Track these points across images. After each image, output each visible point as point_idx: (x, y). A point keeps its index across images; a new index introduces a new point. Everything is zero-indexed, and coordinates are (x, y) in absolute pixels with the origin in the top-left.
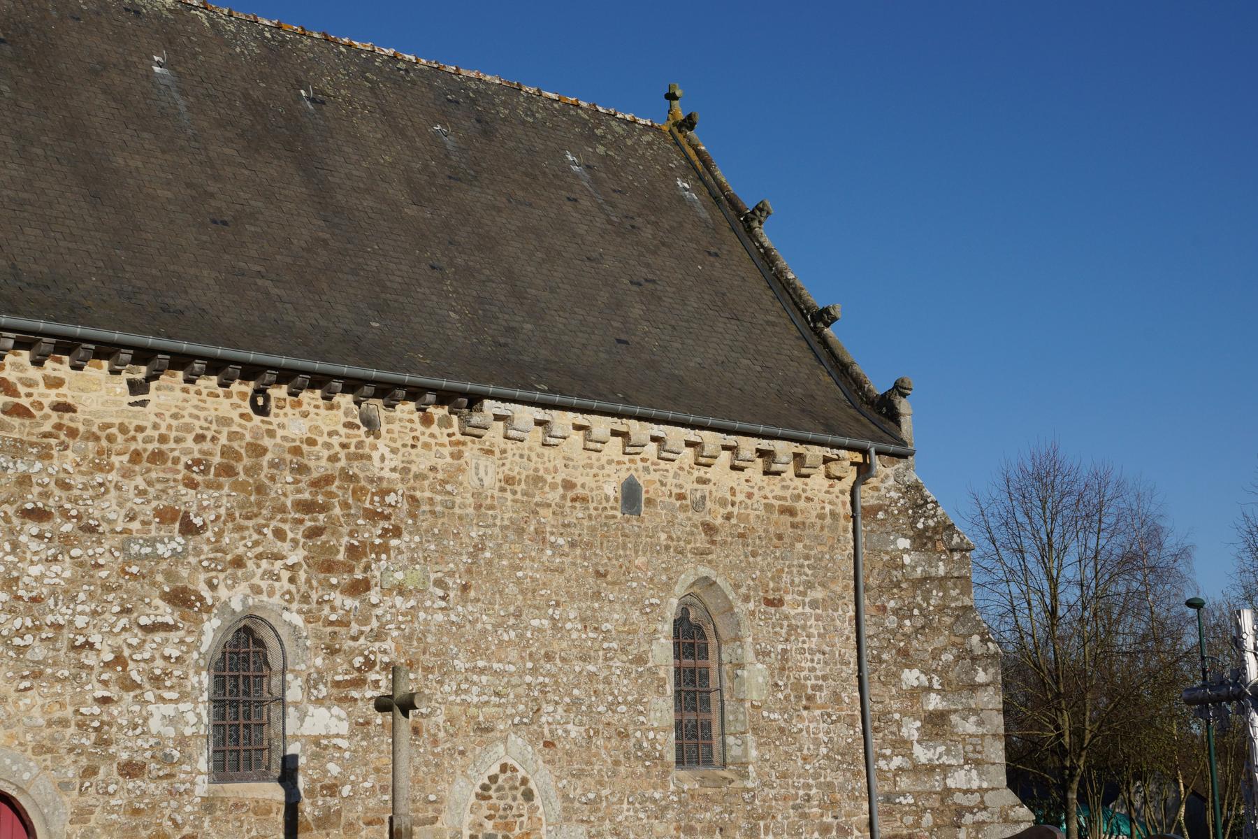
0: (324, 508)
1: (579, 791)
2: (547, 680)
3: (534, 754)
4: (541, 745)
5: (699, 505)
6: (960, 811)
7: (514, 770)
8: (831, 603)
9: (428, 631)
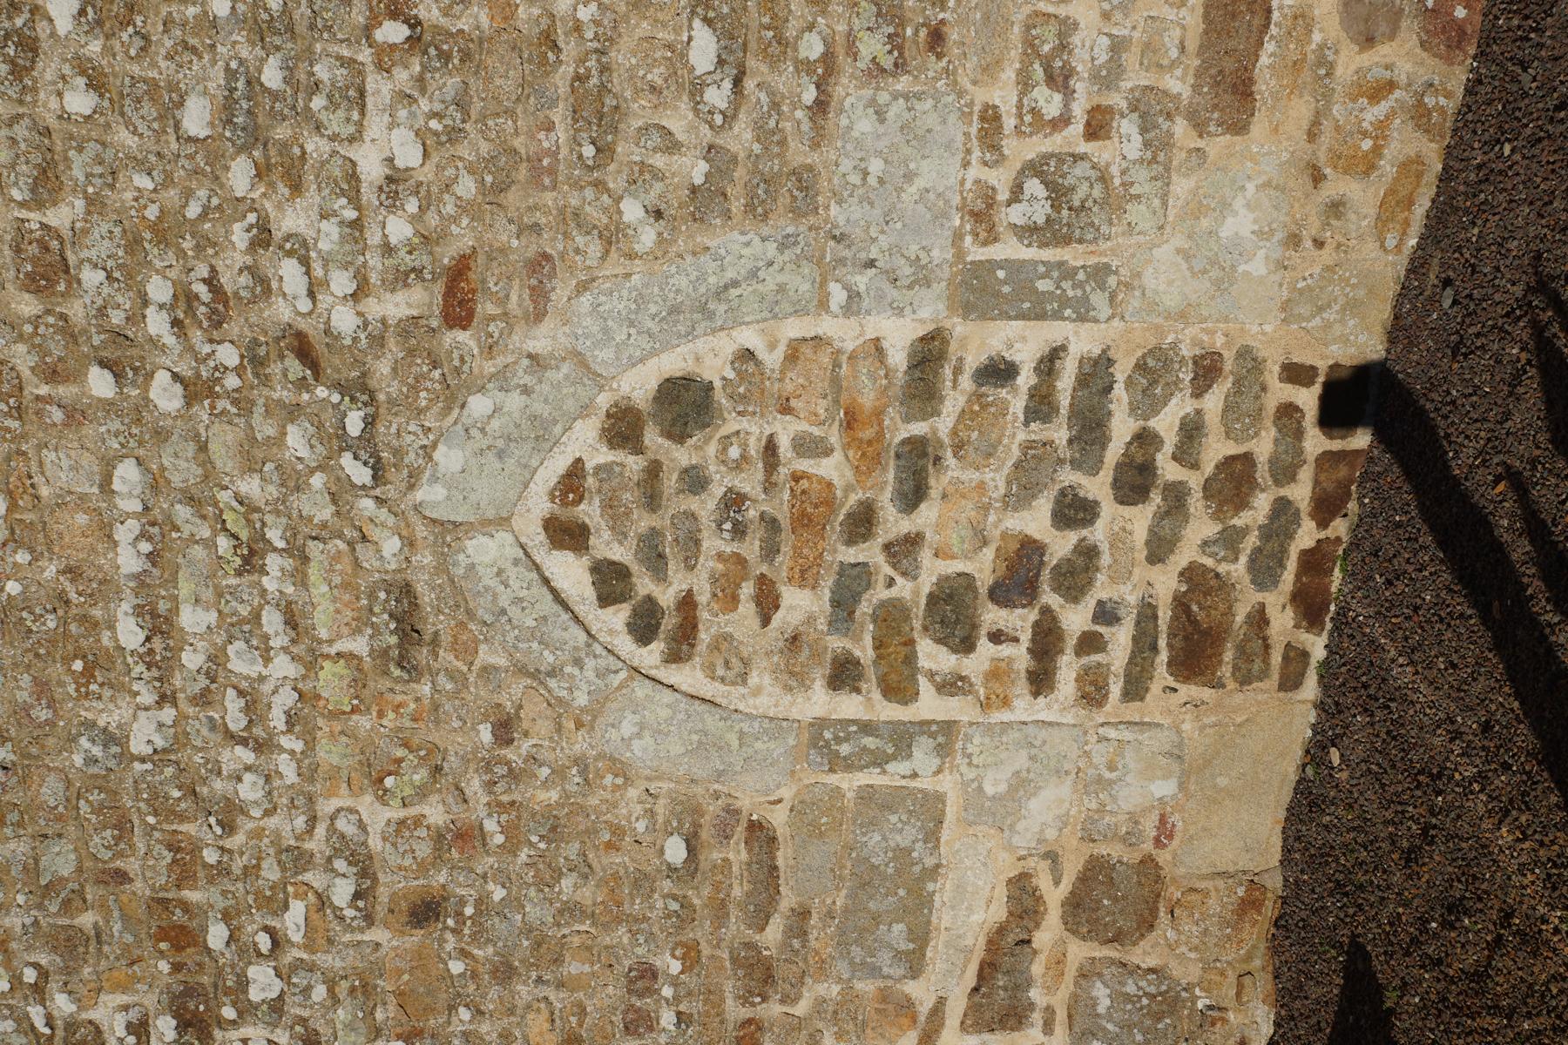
1: (679, 121)
2: (160, 290)
3: (502, 379)
4: (463, 337)
7: (572, 483)
9: (32, 869)
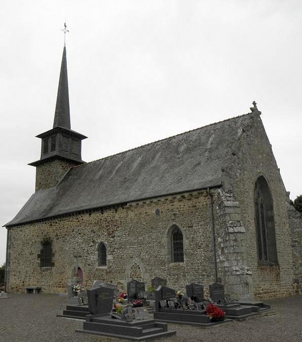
0: (109, 226)
5: (172, 210)
8: (207, 224)
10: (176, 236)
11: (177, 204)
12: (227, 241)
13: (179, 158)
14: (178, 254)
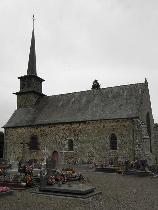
5: (112, 126)
6: (141, 155)
10: (113, 138)
11: (114, 124)
12: (142, 142)
13: (109, 101)
14: (114, 146)
